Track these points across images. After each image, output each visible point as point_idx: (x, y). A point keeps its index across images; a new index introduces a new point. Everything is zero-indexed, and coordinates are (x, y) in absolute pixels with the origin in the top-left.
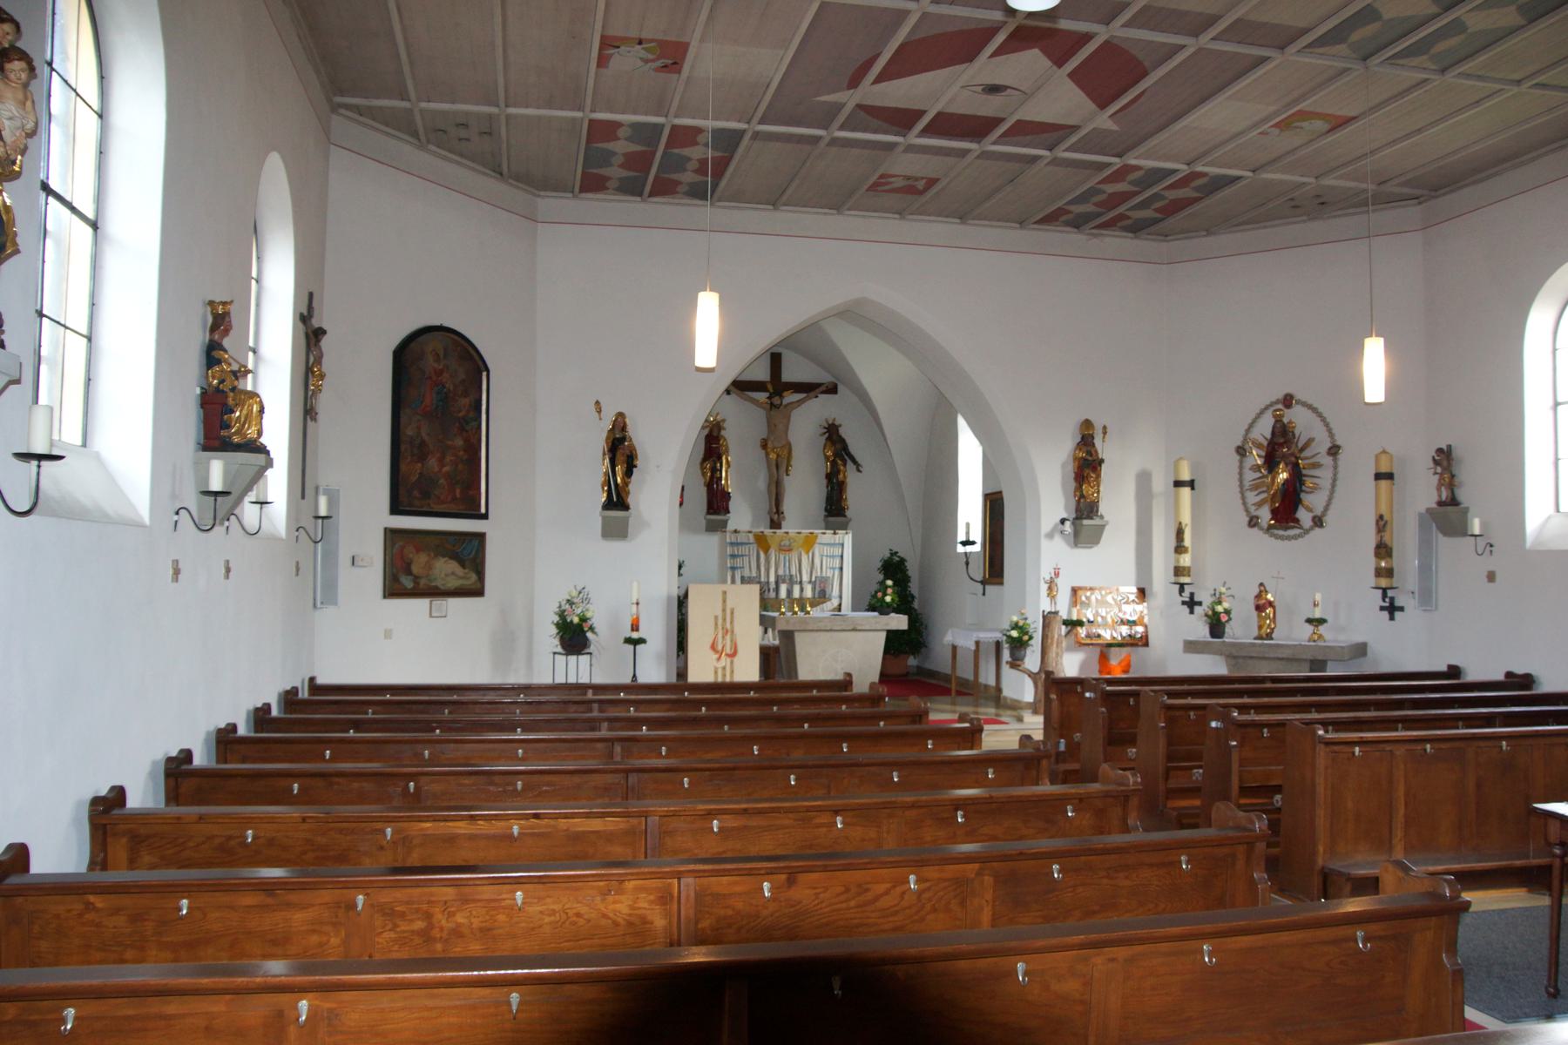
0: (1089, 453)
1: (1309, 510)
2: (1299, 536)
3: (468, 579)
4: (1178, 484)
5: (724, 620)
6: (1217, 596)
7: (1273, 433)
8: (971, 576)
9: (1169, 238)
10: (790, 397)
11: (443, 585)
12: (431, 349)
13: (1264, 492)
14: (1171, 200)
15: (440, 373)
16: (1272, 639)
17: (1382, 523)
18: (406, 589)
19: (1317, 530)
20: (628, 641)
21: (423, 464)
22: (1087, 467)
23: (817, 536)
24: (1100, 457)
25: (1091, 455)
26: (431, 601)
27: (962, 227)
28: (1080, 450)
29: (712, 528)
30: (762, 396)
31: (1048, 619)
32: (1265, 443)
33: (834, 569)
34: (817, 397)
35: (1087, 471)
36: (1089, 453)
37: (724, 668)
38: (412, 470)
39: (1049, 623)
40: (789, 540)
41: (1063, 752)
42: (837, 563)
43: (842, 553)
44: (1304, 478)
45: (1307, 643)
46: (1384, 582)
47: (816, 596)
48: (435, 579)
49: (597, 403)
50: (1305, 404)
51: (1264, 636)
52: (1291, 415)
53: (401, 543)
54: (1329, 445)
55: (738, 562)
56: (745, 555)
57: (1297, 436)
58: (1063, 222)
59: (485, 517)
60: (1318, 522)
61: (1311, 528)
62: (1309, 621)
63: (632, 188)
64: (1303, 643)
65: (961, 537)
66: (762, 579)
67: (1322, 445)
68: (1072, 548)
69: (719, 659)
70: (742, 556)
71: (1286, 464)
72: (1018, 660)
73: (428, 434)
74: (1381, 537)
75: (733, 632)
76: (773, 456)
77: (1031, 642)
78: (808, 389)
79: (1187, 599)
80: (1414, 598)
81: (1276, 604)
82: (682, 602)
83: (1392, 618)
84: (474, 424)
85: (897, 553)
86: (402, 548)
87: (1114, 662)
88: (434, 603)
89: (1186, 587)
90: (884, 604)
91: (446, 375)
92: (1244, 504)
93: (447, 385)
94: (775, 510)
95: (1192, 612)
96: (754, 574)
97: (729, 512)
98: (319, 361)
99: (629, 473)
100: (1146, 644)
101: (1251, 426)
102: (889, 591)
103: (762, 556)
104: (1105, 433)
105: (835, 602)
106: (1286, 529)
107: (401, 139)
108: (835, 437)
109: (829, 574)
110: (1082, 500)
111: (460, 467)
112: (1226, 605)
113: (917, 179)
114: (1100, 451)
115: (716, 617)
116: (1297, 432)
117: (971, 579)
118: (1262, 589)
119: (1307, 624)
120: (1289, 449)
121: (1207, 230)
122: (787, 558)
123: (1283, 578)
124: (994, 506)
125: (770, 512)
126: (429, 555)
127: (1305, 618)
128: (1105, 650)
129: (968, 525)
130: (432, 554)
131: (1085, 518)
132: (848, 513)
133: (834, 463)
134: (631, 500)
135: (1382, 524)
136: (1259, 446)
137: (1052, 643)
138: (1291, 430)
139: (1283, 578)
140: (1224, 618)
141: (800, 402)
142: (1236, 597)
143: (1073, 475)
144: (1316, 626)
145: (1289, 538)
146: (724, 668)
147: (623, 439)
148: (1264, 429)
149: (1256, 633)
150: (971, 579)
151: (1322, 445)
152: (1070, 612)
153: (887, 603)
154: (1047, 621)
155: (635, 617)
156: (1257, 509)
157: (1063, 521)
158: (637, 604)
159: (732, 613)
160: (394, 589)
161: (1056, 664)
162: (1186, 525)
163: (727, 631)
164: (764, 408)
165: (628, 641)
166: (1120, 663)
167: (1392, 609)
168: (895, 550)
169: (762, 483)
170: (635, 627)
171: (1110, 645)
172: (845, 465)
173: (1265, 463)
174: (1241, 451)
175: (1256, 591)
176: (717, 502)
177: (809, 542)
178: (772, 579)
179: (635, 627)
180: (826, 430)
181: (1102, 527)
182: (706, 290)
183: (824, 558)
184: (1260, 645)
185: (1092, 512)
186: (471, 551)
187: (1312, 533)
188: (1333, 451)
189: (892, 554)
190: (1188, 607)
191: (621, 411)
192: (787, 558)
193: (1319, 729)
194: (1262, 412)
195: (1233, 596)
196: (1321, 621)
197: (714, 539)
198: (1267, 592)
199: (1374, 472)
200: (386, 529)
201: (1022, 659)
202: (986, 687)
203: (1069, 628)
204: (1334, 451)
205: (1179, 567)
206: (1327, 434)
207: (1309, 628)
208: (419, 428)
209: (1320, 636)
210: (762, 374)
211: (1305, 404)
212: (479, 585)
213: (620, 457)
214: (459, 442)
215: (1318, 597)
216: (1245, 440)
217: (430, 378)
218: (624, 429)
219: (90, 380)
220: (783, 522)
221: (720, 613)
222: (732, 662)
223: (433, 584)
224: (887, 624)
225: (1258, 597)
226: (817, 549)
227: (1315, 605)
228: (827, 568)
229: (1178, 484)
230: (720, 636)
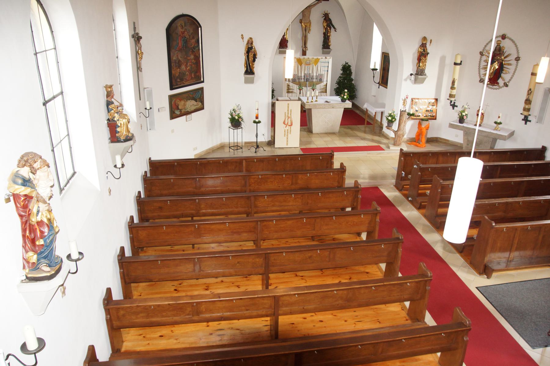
0: (424, 50)
1: (503, 80)
4: (455, 64)
11: (190, 110)
15: (183, 33)
17: (530, 92)
21: (180, 69)
22: (422, 55)
23: (319, 59)
24: (428, 51)
25: (425, 52)
28: (421, 48)
31: (402, 112)
35: (422, 58)
36: (424, 50)
38: (176, 72)
39: (403, 115)
40: (309, 61)
41: (403, 177)
43: (328, 65)
44: (504, 68)
46: (526, 113)
47: (318, 81)
49: (242, 35)
53: (174, 100)
57: (504, 52)
59: (203, 82)
60: (506, 85)
61: (503, 87)
62: (496, 123)
65: (372, 67)
66: (299, 75)
68: (413, 84)
71: (498, 63)
72: (390, 127)
73: (181, 57)
74: (529, 97)
80: (536, 119)
82: (273, 105)
83: (526, 124)
84: (197, 48)
85: (348, 63)
86: (175, 101)
90: (344, 99)
92: (479, 73)
93: (186, 37)
94: (304, 47)
95: (453, 109)
97: (287, 47)
98: (140, 48)
100: (436, 119)
102: (346, 94)
103: (299, 66)
104: (431, 43)
105: (325, 83)
108: (327, 19)
109: (323, 73)
112: (466, 113)
115: (285, 113)
116: (505, 51)
117: (375, 82)
123: (489, 106)
124: (386, 58)
126: (184, 101)
128: (421, 121)
129: (375, 63)
130: (185, 100)
131: (419, 75)
132: (331, 47)
133: (326, 29)
134: (255, 70)
135: (530, 92)
137: (402, 122)
139: (489, 106)
143: (417, 58)
145: (494, 89)
147: (251, 48)
150: (375, 82)
152: (409, 110)
153: (345, 99)
154: (402, 114)
155: (257, 114)
156: (483, 76)
157: (411, 75)
158: (258, 110)
159: (291, 111)
160: (173, 116)
161: (403, 129)
162: (456, 79)
165: (255, 122)
166: (425, 127)
167: (526, 120)
169: (300, 36)
170: (257, 118)
171: (422, 120)
172: (330, 29)
177: (317, 61)
178: (303, 75)
179: (257, 118)
180: (324, 14)
181: (425, 78)
182: (482, 177)
183: (322, 67)
185: (422, 73)
188: (517, 59)
189: (346, 64)
193: (493, 223)
196: (500, 123)
199: (531, 72)
200: (169, 96)
201: (391, 127)
202: (377, 120)
204: (518, 59)
207: (495, 125)
208: (177, 56)
214: (192, 57)
215: (500, 116)
216: (484, 50)
217: (180, 35)
218: (252, 43)
219: (53, 32)
220: (307, 51)
221: (289, 135)
222: (290, 128)
223: (187, 110)
224: (345, 106)
226: (319, 64)
229: (455, 64)
230: (286, 119)
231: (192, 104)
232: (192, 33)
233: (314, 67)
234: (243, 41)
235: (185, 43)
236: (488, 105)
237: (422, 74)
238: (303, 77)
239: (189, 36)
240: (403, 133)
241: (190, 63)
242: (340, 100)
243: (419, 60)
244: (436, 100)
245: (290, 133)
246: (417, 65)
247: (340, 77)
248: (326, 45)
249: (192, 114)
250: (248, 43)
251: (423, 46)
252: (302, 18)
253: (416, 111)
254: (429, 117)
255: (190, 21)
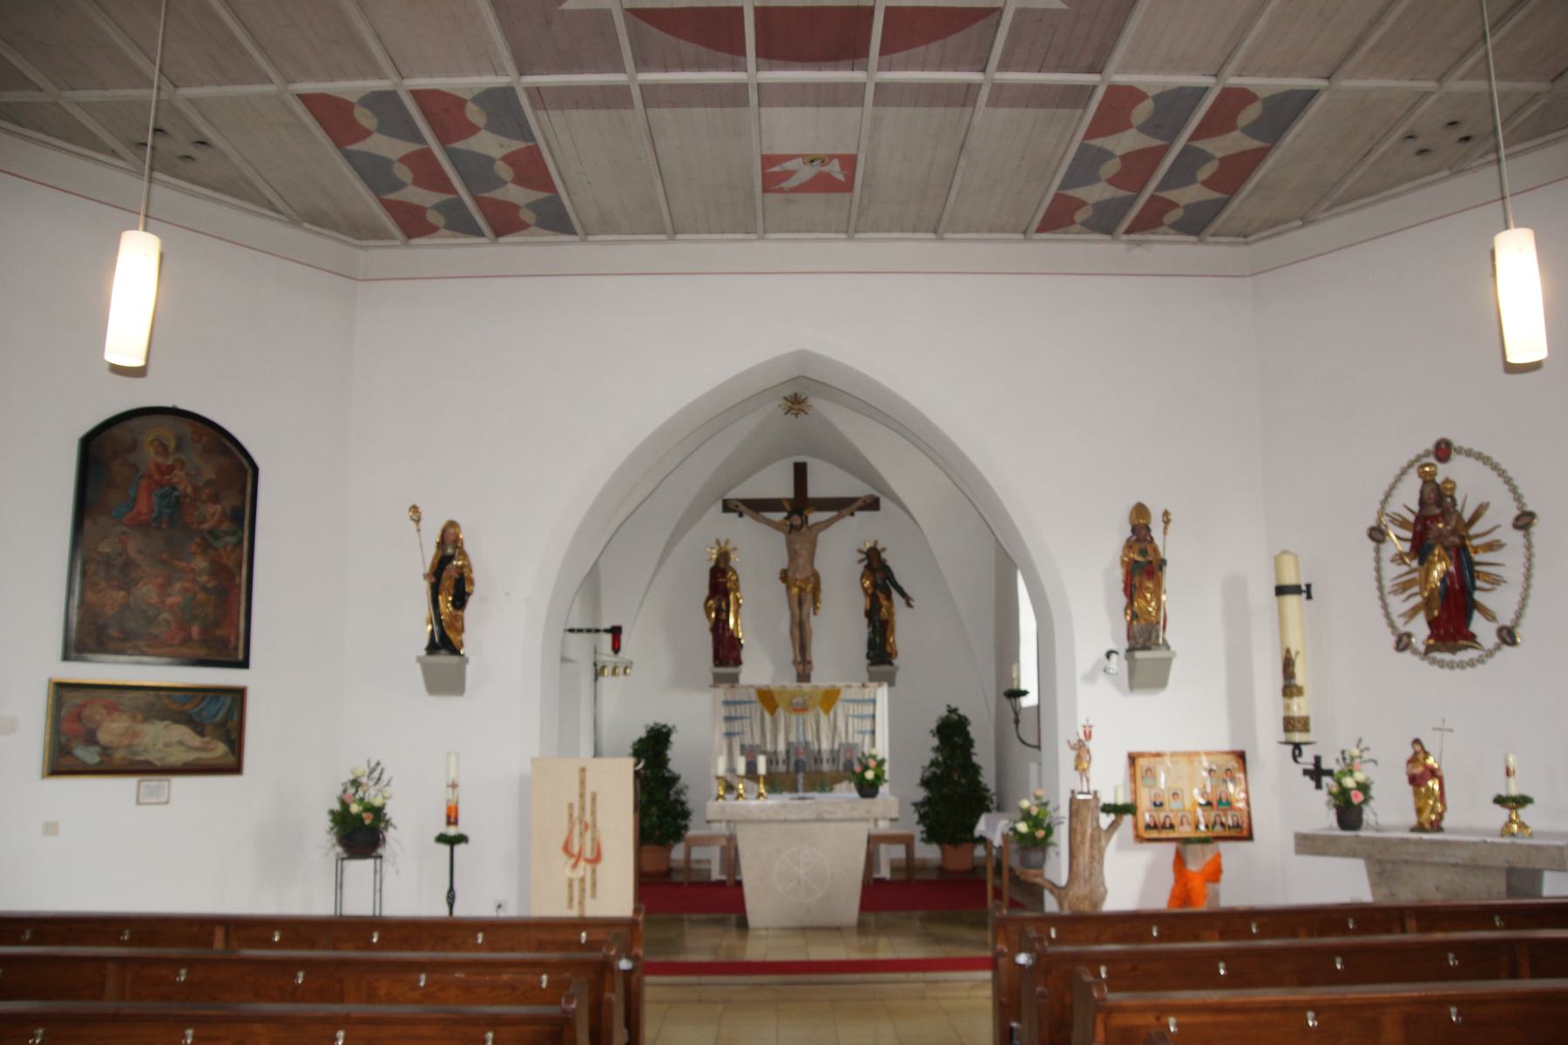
0: (1143, 552)
1: (1489, 615)
2: (1481, 660)
3: (212, 750)
4: (1281, 590)
5: (583, 809)
6: (1348, 761)
7: (1422, 502)
8: (1024, 738)
9: (1250, 239)
10: (815, 517)
11: (160, 759)
12: (151, 438)
13: (1414, 595)
14: (1222, 160)
16: (1439, 829)
18: (84, 763)
19: (1507, 650)
20: (442, 839)
21: (129, 595)
26: (139, 782)
27: (938, 245)
29: (718, 680)
30: (779, 516)
32: (1411, 518)
33: (862, 733)
34: (852, 514)
37: (582, 880)
42: (867, 725)
44: (1478, 568)
45: (1498, 840)
47: (841, 768)
48: (146, 750)
49: (414, 509)
50: (1469, 453)
51: (1427, 826)
52: (1443, 472)
54: (1516, 513)
55: (737, 726)
56: (745, 718)
58: (1083, 224)
59: (244, 664)
60: (1508, 636)
61: (1498, 648)
62: (1500, 801)
63: (1105, 222)
64: (1489, 839)
67: (1501, 514)
69: (575, 866)
70: (741, 718)
71: (1446, 549)
73: (140, 552)
75: (594, 826)
76: (795, 590)
77: (1053, 839)
78: (842, 506)
79: (1311, 767)
81: (1445, 773)
87: (1194, 866)
88: (144, 784)
89: (1304, 748)
90: (864, 784)
91: (178, 475)
92: (1387, 615)
93: (181, 487)
96: (757, 741)
99: (460, 600)
100: (1249, 837)
101: (1388, 495)
104: (1167, 522)
106: (1454, 650)
107: (14, 132)
109: (857, 739)
110: (1135, 623)
111: (201, 596)
112: (1360, 776)
113: (824, 160)
114: (1161, 549)
115: (571, 806)
118: (1419, 751)
119: (1497, 808)
120: (1446, 524)
121: (1301, 219)
122: (801, 720)
123: (1451, 730)
125: (795, 662)
127: (1493, 795)
128: (1181, 846)
130: (140, 717)
132: (896, 662)
134: (471, 641)
136: (1403, 524)
137: (1083, 842)
138: (1449, 493)
139: (1451, 730)
140: (1357, 798)
141: (829, 523)
142: (1379, 762)
144: (1511, 808)
145: (1461, 665)
146: (582, 880)
148: (1408, 498)
149: (1412, 820)
150: (1023, 742)
151: (1501, 514)
153: (867, 781)
154: (1074, 807)
156: (1406, 623)
157: (1109, 654)
159: (594, 799)
160: (61, 763)
162: (1297, 653)
163: (586, 826)
164: (782, 530)
165: (442, 839)
168: (953, 706)
170: (452, 820)
171: (1186, 841)
172: (889, 598)
173: (1413, 548)
174: (1377, 535)
175: (1409, 752)
176: (726, 650)
177: (830, 698)
178: (782, 747)
179: (452, 820)
181: (1167, 663)
182: (137, 229)
183: (850, 720)
184: (1419, 842)
185: (1149, 638)
186: (220, 709)
187: (1499, 654)
188: (1523, 522)
190: (1312, 778)
191: (457, 520)
192: (801, 720)
194: (1404, 472)
195: (1375, 762)
196: (1522, 801)
197: (722, 693)
198: (1426, 754)
200: (50, 680)
203: (1112, 817)
204: (1524, 521)
205: (1293, 718)
206: (1510, 495)
207: (1502, 814)
209: (1522, 826)
210: (783, 488)
211: (1469, 453)
212: (231, 760)
213: (447, 583)
222: (594, 872)
223: (141, 758)
225: (1413, 761)
226: (840, 708)
227: (1508, 773)
228: (854, 731)
229: (1281, 590)
231: (175, 739)
232: (209, 483)
233: (824, 722)
234: (419, 530)
235: (168, 506)
236: (1447, 726)
237: (1148, 644)
238: (782, 756)
239: (195, 487)
240: (1092, 891)
241: (187, 585)
242: (855, 795)
243: (1131, 590)
244: (1241, 756)
245: (594, 895)
246: (1126, 614)
247: (934, 763)
248: (880, 653)
249: (179, 783)
250: (442, 544)
251: (1140, 533)
252: (789, 566)
253: (1155, 804)
254: (1218, 828)
255: (204, 439)
